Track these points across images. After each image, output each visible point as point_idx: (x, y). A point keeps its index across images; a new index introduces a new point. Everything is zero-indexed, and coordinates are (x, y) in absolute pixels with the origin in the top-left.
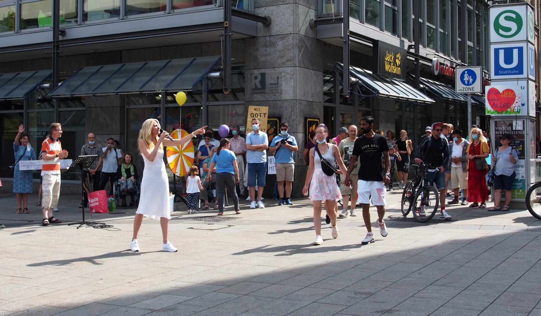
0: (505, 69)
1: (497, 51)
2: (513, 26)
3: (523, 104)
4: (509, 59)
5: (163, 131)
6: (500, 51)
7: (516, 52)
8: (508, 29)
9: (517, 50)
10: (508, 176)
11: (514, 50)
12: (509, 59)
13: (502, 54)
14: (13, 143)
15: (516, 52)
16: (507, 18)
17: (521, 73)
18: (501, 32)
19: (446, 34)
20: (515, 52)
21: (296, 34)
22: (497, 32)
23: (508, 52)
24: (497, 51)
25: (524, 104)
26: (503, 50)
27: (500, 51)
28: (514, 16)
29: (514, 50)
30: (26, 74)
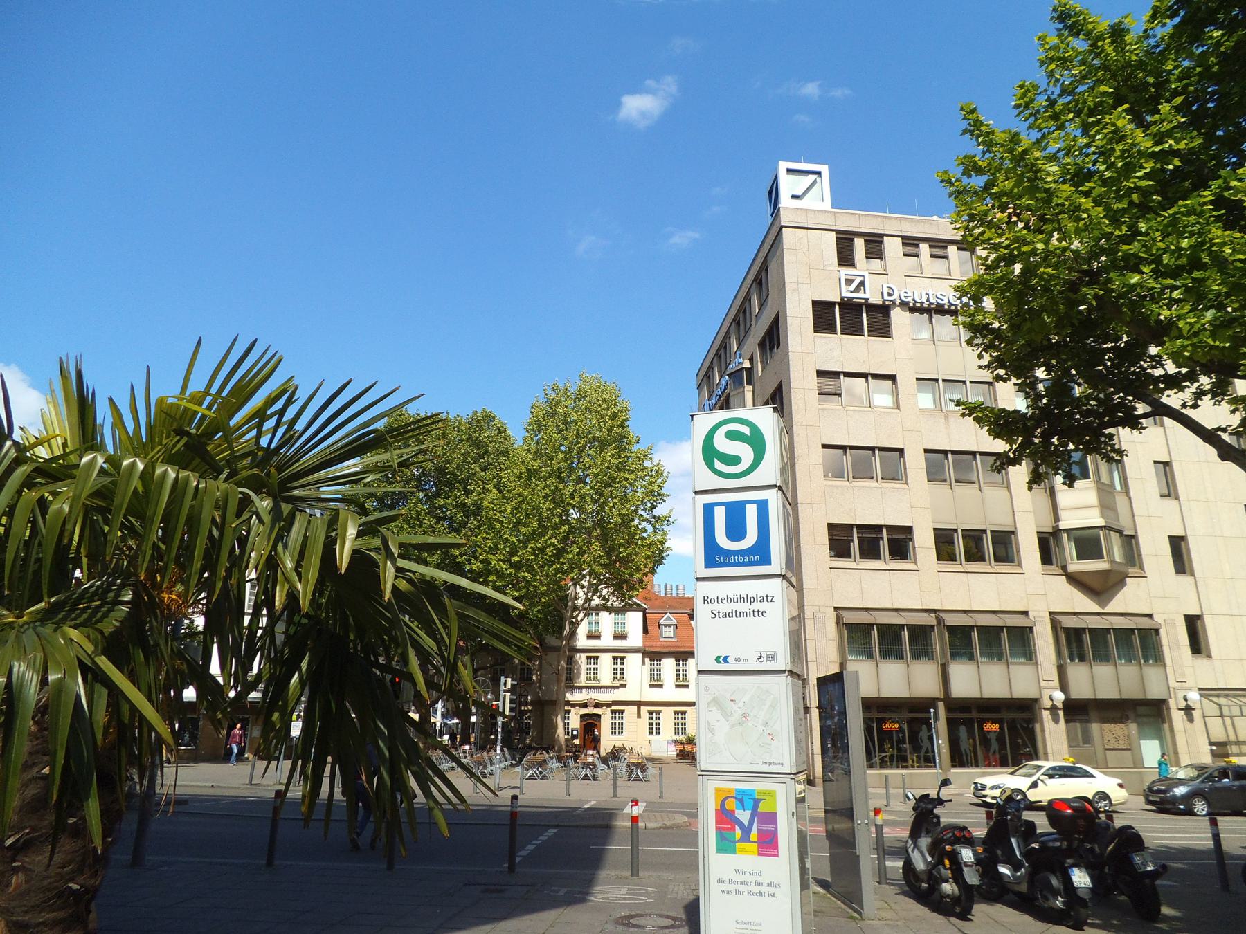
0: (729, 553)
2: (745, 452)
3: (728, 660)
4: (736, 529)
5: (905, 743)
6: (748, 506)
7: (751, 512)
8: (734, 460)
9: (754, 506)
10: (1073, 883)
11: (747, 506)
12: (736, 529)
14: (949, 860)
15: (751, 512)
16: (731, 436)
17: (766, 560)
18: (719, 465)
19: (206, 487)
20: (751, 512)
21: (55, 437)
22: (711, 466)
23: (736, 514)
25: (728, 663)
26: (724, 507)
27: (748, 506)
28: (745, 430)
29: (747, 506)
30: (380, 425)
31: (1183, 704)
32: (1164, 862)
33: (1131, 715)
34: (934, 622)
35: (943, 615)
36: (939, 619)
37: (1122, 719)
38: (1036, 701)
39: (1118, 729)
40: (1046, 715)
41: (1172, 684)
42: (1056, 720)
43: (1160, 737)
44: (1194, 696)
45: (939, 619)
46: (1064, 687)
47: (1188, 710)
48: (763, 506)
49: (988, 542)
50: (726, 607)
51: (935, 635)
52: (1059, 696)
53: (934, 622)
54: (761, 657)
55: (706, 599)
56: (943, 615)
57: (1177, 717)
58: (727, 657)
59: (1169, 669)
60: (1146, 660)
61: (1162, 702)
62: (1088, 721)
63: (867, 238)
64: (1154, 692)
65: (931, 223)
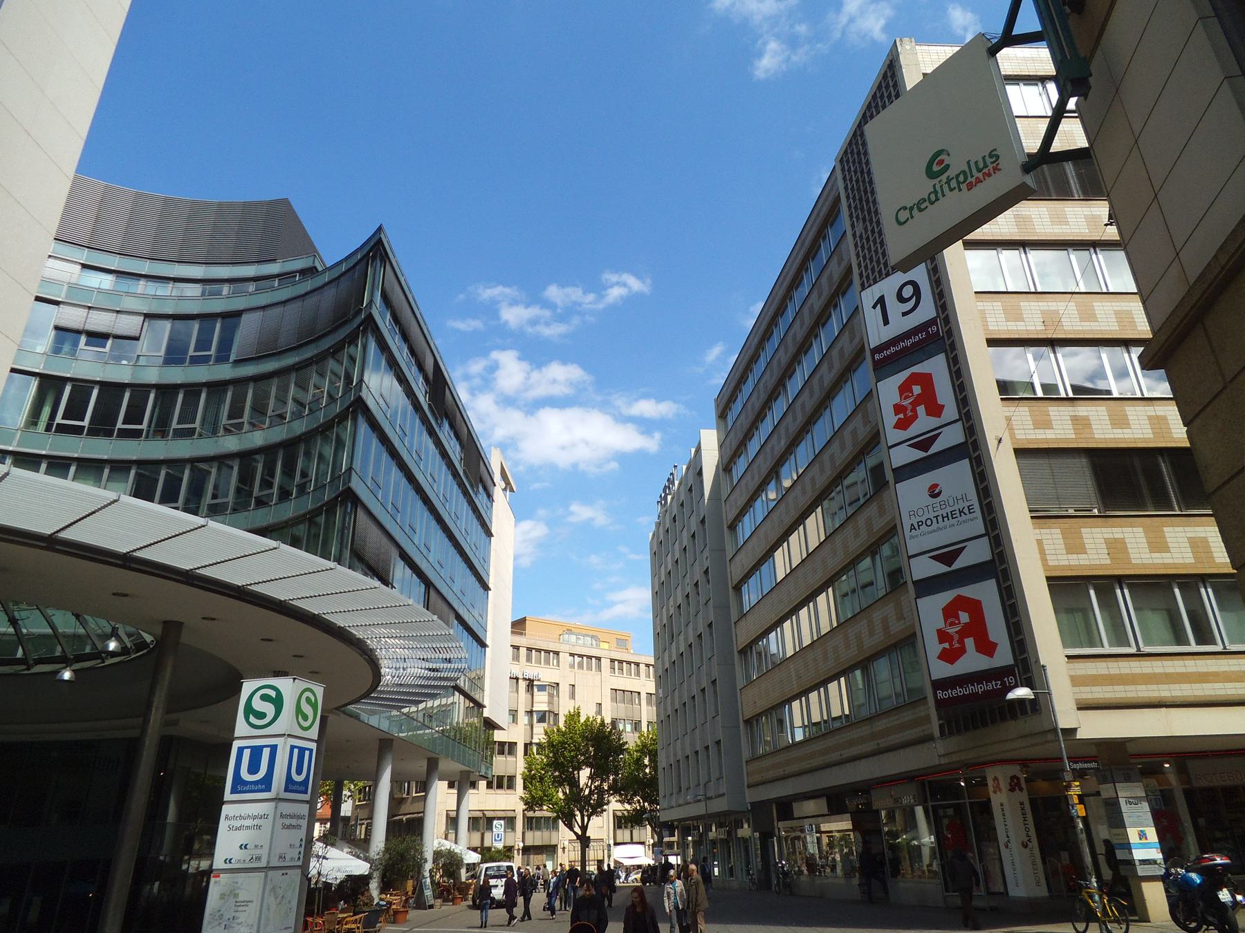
1: (241, 750)
12: (253, 769)
13: (247, 753)
16: (265, 698)
17: (268, 789)
24: (241, 750)
31: (562, 846)
32: (746, 787)
33: (545, 851)
34: (482, 815)
35: (485, 812)
36: (484, 814)
37: (541, 853)
38: (513, 847)
39: (539, 857)
40: (516, 852)
41: (560, 838)
42: (519, 855)
43: (553, 860)
44: (566, 843)
45: (484, 814)
46: (523, 841)
47: (564, 848)
48: (274, 749)
49: (505, 780)
50: (238, 823)
51: (481, 821)
52: (521, 845)
53: (482, 815)
54: (252, 858)
55: (227, 817)
56: (485, 812)
57: (560, 851)
58: (231, 859)
59: (560, 832)
60: (553, 828)
61: (557, 845)
62: (530, 855)
63: (113, 465)
64: (553, 843)
65: (267, 515)
